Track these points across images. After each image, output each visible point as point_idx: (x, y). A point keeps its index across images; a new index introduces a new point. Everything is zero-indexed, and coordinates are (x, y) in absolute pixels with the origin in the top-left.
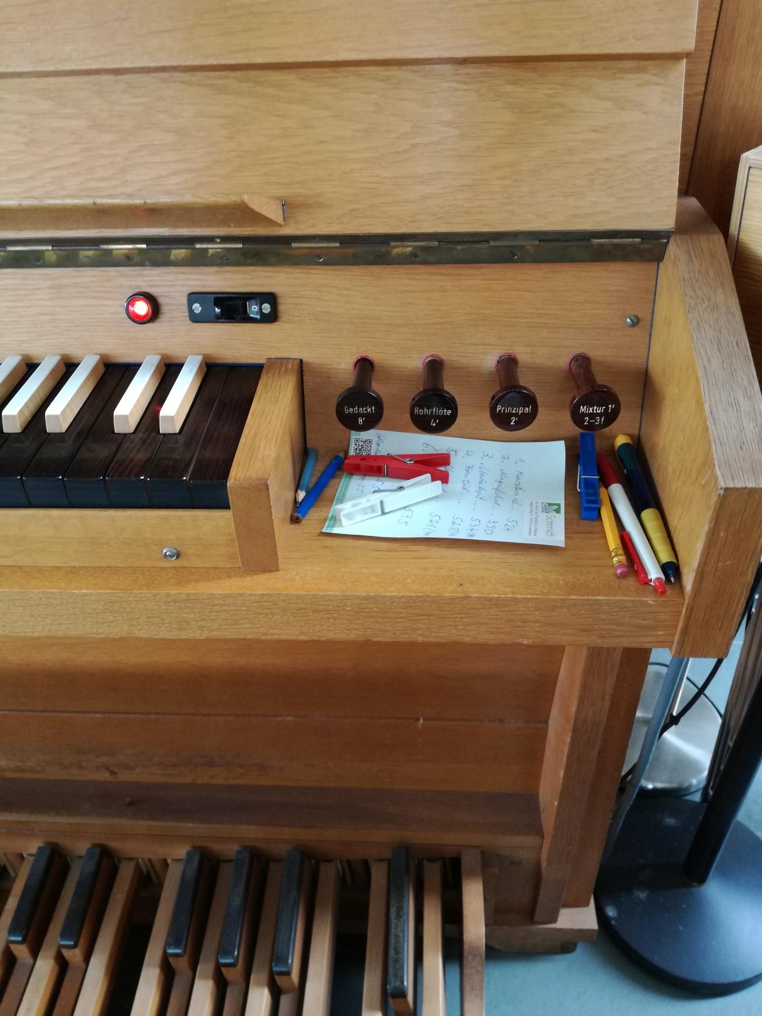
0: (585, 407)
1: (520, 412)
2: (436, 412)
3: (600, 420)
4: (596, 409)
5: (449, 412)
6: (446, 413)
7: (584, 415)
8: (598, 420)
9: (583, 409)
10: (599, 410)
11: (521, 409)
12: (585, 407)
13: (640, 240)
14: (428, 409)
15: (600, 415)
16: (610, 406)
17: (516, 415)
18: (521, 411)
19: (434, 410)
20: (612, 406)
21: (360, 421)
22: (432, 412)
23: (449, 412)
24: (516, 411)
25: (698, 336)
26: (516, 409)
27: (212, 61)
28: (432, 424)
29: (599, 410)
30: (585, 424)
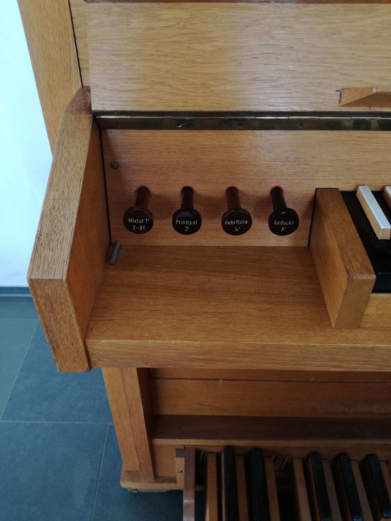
0: (131, 219)
1: (190, 224)
2: (238, 222)
3: (143, 228)
4: (138, 221)
5: (246, 222)
6: (245, 222)
7: (132, 224)
8: (141, 227)
9: (130, 220)
10: (140, 222)
11: (191, 222)
12: (131, 219)
13: (96, 117)
14: (233, 221)
15: (141, 224)
16: (146, 219)
17: (188, 225)
18: (191, 223)
19: (237, 221)
20: (147, 220)
21: (283, 229)
22: (236, 223)
23: (246, 222)
24: (188, 223)
25: (276, 179)
26: (188, 222)
27: (74, 44)
28: (236, 230)
29: (184, 222)
30: (186, 230)
